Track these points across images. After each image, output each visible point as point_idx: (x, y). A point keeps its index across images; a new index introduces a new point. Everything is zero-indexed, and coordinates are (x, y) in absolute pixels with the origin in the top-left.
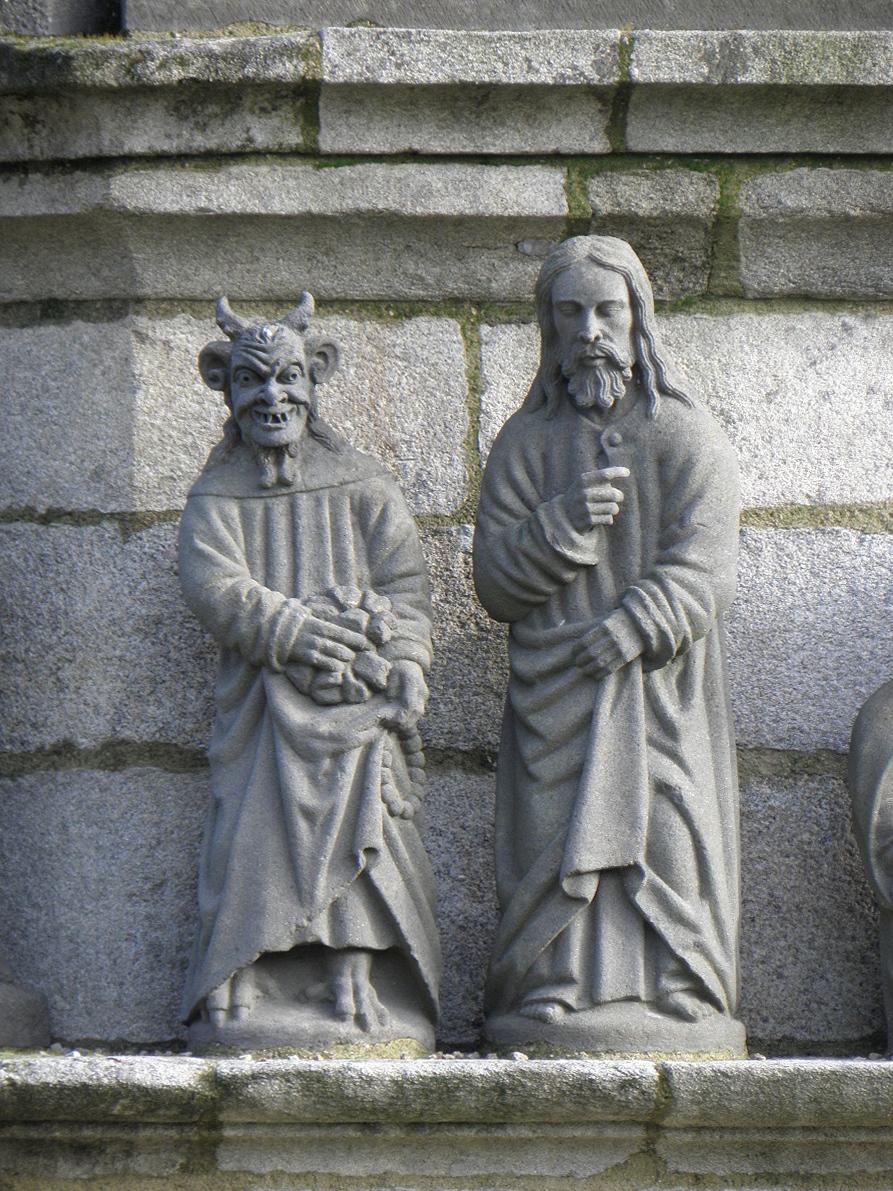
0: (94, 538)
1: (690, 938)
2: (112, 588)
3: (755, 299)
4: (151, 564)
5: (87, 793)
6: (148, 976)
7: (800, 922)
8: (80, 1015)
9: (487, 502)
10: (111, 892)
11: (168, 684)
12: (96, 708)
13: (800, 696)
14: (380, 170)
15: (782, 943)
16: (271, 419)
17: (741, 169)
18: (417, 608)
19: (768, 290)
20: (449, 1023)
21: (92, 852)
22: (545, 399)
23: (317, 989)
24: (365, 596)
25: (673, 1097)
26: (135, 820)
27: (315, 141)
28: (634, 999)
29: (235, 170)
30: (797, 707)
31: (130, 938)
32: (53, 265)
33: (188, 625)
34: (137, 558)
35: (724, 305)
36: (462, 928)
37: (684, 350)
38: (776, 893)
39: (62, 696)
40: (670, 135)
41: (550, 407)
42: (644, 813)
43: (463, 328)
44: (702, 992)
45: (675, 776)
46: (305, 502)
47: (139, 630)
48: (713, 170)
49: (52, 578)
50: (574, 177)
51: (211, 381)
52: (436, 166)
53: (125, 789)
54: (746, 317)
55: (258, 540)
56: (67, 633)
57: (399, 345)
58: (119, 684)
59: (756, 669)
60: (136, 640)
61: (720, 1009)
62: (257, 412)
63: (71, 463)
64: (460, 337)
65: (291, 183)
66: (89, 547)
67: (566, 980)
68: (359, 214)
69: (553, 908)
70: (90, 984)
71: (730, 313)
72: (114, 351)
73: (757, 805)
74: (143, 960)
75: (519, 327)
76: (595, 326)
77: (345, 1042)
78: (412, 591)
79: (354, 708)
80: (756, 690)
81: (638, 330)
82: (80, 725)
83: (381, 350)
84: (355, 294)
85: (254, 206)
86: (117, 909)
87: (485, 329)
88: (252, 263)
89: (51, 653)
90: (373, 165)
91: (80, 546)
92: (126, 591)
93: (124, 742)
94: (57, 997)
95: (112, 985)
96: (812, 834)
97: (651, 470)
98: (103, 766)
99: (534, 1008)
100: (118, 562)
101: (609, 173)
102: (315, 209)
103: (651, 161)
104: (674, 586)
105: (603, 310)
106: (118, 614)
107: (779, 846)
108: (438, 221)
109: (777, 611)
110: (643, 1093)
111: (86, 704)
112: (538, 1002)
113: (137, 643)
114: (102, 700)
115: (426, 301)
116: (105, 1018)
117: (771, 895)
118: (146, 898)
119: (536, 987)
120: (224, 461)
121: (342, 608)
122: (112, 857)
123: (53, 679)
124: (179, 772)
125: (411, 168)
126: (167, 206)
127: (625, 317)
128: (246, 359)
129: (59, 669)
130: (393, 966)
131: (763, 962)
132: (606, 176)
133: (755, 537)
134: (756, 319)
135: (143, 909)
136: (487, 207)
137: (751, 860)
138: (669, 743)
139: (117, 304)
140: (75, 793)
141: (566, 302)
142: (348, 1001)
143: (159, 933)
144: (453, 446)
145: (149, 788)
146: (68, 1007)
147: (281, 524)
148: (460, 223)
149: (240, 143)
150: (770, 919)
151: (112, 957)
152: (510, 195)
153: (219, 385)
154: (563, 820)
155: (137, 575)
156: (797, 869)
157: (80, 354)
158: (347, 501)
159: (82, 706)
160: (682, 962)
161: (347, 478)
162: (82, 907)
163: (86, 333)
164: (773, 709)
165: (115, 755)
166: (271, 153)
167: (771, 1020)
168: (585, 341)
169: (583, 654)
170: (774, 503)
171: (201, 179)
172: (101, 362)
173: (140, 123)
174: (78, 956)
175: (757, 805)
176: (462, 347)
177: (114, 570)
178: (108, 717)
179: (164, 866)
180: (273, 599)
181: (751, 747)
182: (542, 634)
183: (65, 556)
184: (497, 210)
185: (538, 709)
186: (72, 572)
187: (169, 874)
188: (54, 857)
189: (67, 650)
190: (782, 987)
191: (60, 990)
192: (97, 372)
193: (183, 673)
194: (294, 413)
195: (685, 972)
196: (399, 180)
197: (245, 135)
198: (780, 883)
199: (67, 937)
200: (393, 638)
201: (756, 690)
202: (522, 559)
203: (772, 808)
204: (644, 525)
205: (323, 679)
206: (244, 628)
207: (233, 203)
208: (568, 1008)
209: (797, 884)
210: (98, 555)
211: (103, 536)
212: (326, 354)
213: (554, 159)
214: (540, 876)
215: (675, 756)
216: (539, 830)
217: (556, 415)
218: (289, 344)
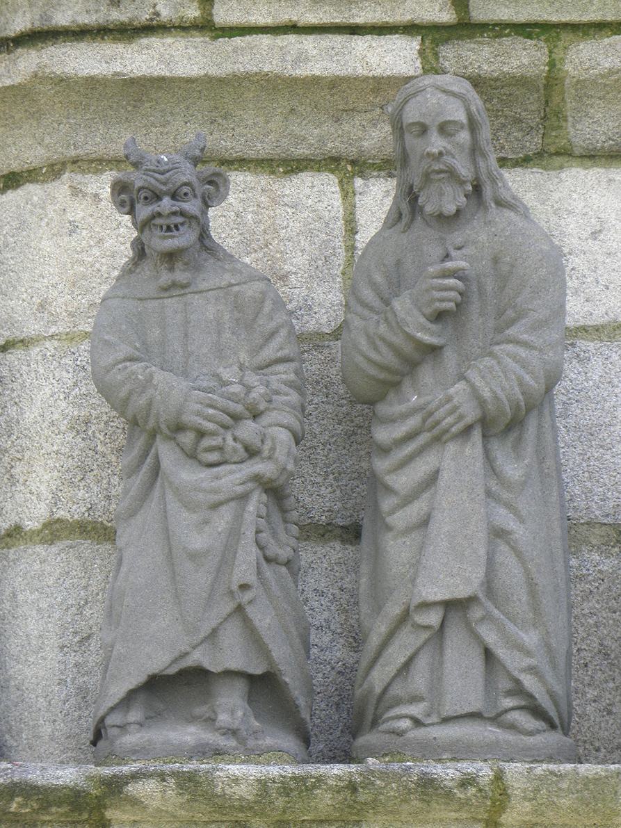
0: (39, 358)
2: (52, 396)
3: (582, 157)
5: (31, 566)
6: (76, 714)
8: (24, 750)
9: (353, 302)
10: (47, 646)
11: (95, 472)
14: (266, 40)
17: (566, 37)
18: (290, 387)
19: (591, 147)
20: (331, 754)
21: (34, 613)
22: (400, 215)
25: (506, 794)
26: (67, 584)
27: (211, 15)
28: (474, 716)
29: (145, 41)
32: (10, 141)
33: (112, 424)
34: (70, 370)
35: (558, 160)
36: (339, 672)
38: (605, 643)
39: (13, 488)
40: (506, 6)
41: (404, 220)
43: (341, 182)
47: (72, 428)
48: (543, 38)
49: (9, 395)
50: (427, 43)
52: (313, 37)
53: (59, 558)
54: (574, 171)
56: (18, 438)
57: (287, 196)
58: (56, 474)
59: (586, 457)
60: (70, 436)
62: (154, 225)
63: (24, 300)
64: (338, 189)
65: (192, 51)
66: (35, 365)
68: (248, 77)
70: (31, 723)
71: (561, 167)
72: (55, 205)
73: (588, 570)
74: (72, 700)
75: (387, 180)
80: (586, 475)
82: (27, 511)
83: (274, 200)
84: (252, 154)
85: (160, 70)
86: (52, 659)
87: (358, 182)
88: (164, 126)
89: (7, 455)
90: (260, 36)
91: (29, 366)
92: (61, 397)
93: (59, 521)
94: (7, 737)
95: (47, 723)
98: (44, 541)
99: (389, 724)
100: (56, 375)
101: (456, 42)
102: (213, 71)
103: (490, 30)
106: (56, 416)
107: (607, 603)
108: (314, 81)
109: (603, 409)
110: (480, 790)
112: (393, 718)
113: (70, 439)
114: (43, 488)
115: (311, 160)
116: (42, 751)
117: (601, 645)
118: (76, 648)
119: (391, 707)
120: (131, 272)
122: (49, 617)
123: (8, 476)
125: (292, 38)
127: (464, 136)
129: (12, 467)
130: (264, 687)
131: (595, 701)
132: (454, 45)
133: (584, 348)
134: (582, 172)
135: (72, 658)
136: (354, 70)
137: (584, 615)
139: (56, 168)
140: (22, 567)
141: (413, 124)
143: (86, 678)
144: (333, 277)
145: (79, 558)
146: (15, 744)
148: (335, 84)
149: (148, 17)
150: (601, 664)
151: (47, 700)
152: (373, 59)
153: (127, 209)
154: (413, 561)
155: (70, 383)
157: (31, 212)
159: (28, 495)
160: (517, 682)
161: (233, 281)
162: (26, 660)
163: (36, 195)
164: (601, 490)
165: (54, 531)
166: (175, 27)
167: (603, 750)
169: (430, 420)
170: (600, 321)
171: (119, 48)
172: (46, 215)
173: (85, 39)
174: (22, 701)
175: (588, 570)
176: (338, 196)
177: (54, 381)
178: (48, 501)
179: (91, 622)
181: (582, 521)
182: (398, 409)
183: (18, 375)
184: (361, 71)
186: (23, 386)
187: (94, 629)
188: (6, 621)
189: (18, 452)
190: (611, 721)
191: (9, 731)
192: (43, 224)
193: (108, 463)
194: (186, 226)
196: (281, 48)
197: (152, 10)
198: (608, 635)
199: (16, 685)
200: (267, 409)
201: (586, 475)
202: (379, 343)
203: (600, 572)
210: (42, 371)
211: (45, 355)
213: (409, 29)
216: (393, 570)
217: (409, 228)
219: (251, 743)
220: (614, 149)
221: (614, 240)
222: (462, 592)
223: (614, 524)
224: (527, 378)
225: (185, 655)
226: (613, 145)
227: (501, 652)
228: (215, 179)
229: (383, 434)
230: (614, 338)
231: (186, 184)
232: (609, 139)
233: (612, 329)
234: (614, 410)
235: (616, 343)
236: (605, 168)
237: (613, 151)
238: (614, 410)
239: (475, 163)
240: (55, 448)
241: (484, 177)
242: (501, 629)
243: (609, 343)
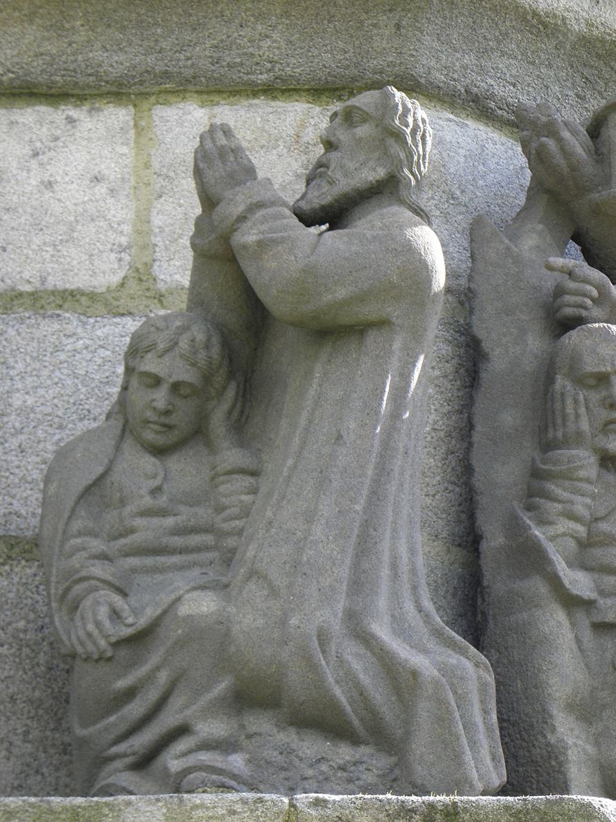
7: (14, 713)
13: (17, 481)
96: (28, 622)
156: (11, 659)
209: (12, 673)
220: (15, 84)
221: (14, 193)
223: (4, 536)
226: (14, 79)
230: (11, 309)
232: (9, 71)
233: (9, 299)
234: (8, 397)
235: (13, 316)
236: (6, 108)
237: (15, 88)
238: (8, 397)
243: (4, 316)
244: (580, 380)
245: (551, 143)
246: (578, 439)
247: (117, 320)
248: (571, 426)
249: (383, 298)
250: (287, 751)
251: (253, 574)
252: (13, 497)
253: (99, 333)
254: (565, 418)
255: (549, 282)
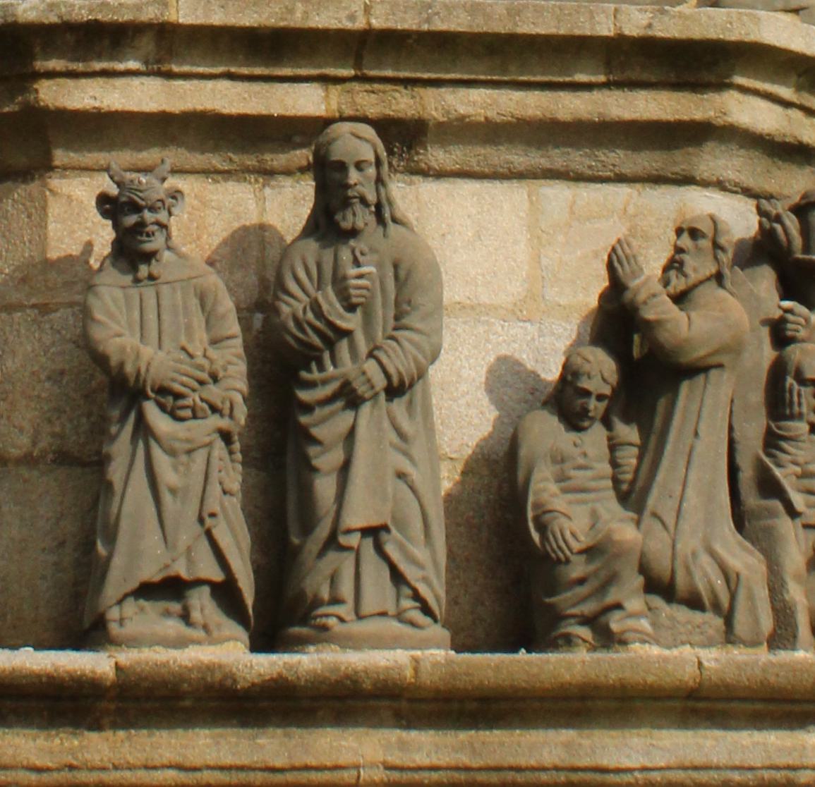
1: (420, 573)
4: (58, 336)
12: (21, 430)
13: (466, 425)
15: (457, 582)
16: (144, 235)
23: (176, 607)
24: (205, 350)
28: (383, 614)
30: (464, 431)
31: (44, 577)
37: (408, 195)
42: (390, 490)
44: (426, 610)
45: (407, 467)
46: (165, 290)
51: (105, 214)
55: (136, 314)
61: (436, 621)
67: (336, 601)
69: (332, 556)
76: (354, 176)
77: (198, 642)
78: (235, 347)
79: (199, 422)
81: (379, 181)
97: (390, 273)
104: (406, 344)
105: (359, 166)
106: (36, 368)
111: (14, 426)
112: (321, 616)
121: (191, 356)
124: (521, 155)
126: (75, 104)
127: (371, 171)
128: (129, 197)
130: (226, 594)
138: (403, 446)
142: (196, 615)
147: (151, 303)
158: (192, 291)
168: (348, 186)
180: (148, 351)
185: (316, 425)
195: (416, 596)
200: (224, 377)
202: (306, 326)
204: (384, 305)
205: (181, 402)
206: (129, 369)
207: (117, 104)
208: (342, 620)
212: (176, 195)
214: (323, 531)
215: (406, 454)
218: (152, 187)
219: (215, 634)
222: (374, 521)
224: (420, 357)
225: (167, 566)
227: (404, 567)
228: (176, 194)
229: (304, 395)
231: (159, 200)
239: (377, 190)
240: (36, 393)
241: (384, 201)
242: (402, 548)
244: (802, 381)
245: (778, 227)
246: (800, 416)
247: (521, 324)
248: (796, 409)
249: (482, 164)
250: (672, 618)
251: (655, 515)
252: (464, 434)
253: (511, 332)
254: (791, 402)
255: (778, 314)
